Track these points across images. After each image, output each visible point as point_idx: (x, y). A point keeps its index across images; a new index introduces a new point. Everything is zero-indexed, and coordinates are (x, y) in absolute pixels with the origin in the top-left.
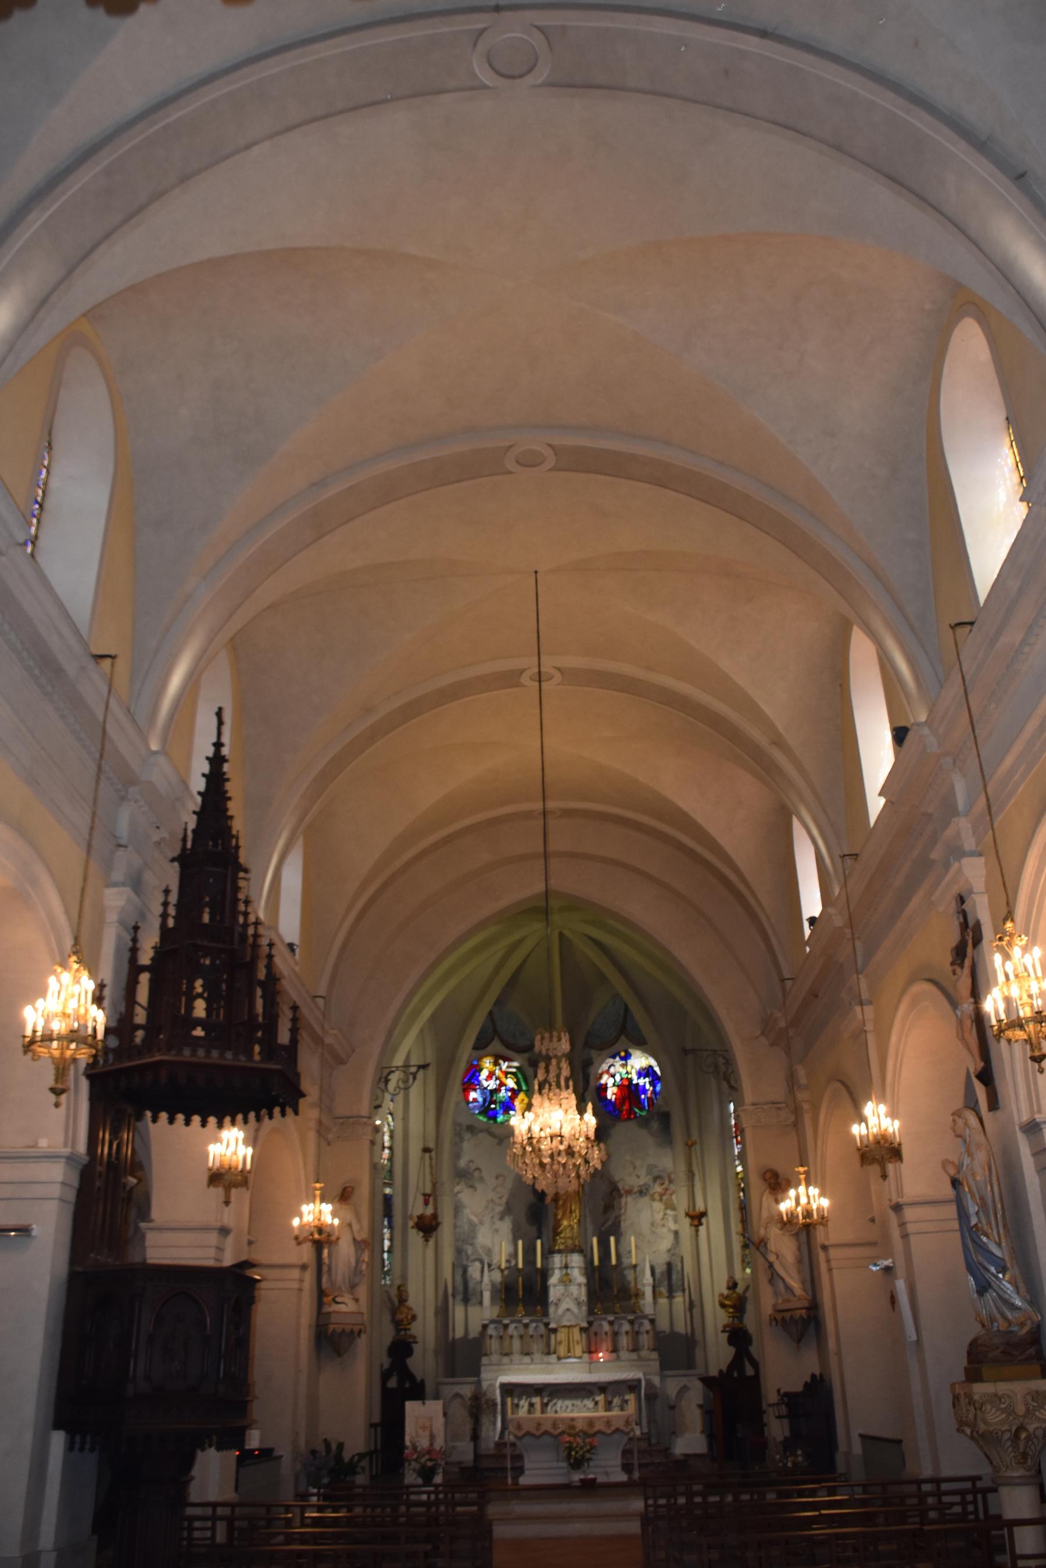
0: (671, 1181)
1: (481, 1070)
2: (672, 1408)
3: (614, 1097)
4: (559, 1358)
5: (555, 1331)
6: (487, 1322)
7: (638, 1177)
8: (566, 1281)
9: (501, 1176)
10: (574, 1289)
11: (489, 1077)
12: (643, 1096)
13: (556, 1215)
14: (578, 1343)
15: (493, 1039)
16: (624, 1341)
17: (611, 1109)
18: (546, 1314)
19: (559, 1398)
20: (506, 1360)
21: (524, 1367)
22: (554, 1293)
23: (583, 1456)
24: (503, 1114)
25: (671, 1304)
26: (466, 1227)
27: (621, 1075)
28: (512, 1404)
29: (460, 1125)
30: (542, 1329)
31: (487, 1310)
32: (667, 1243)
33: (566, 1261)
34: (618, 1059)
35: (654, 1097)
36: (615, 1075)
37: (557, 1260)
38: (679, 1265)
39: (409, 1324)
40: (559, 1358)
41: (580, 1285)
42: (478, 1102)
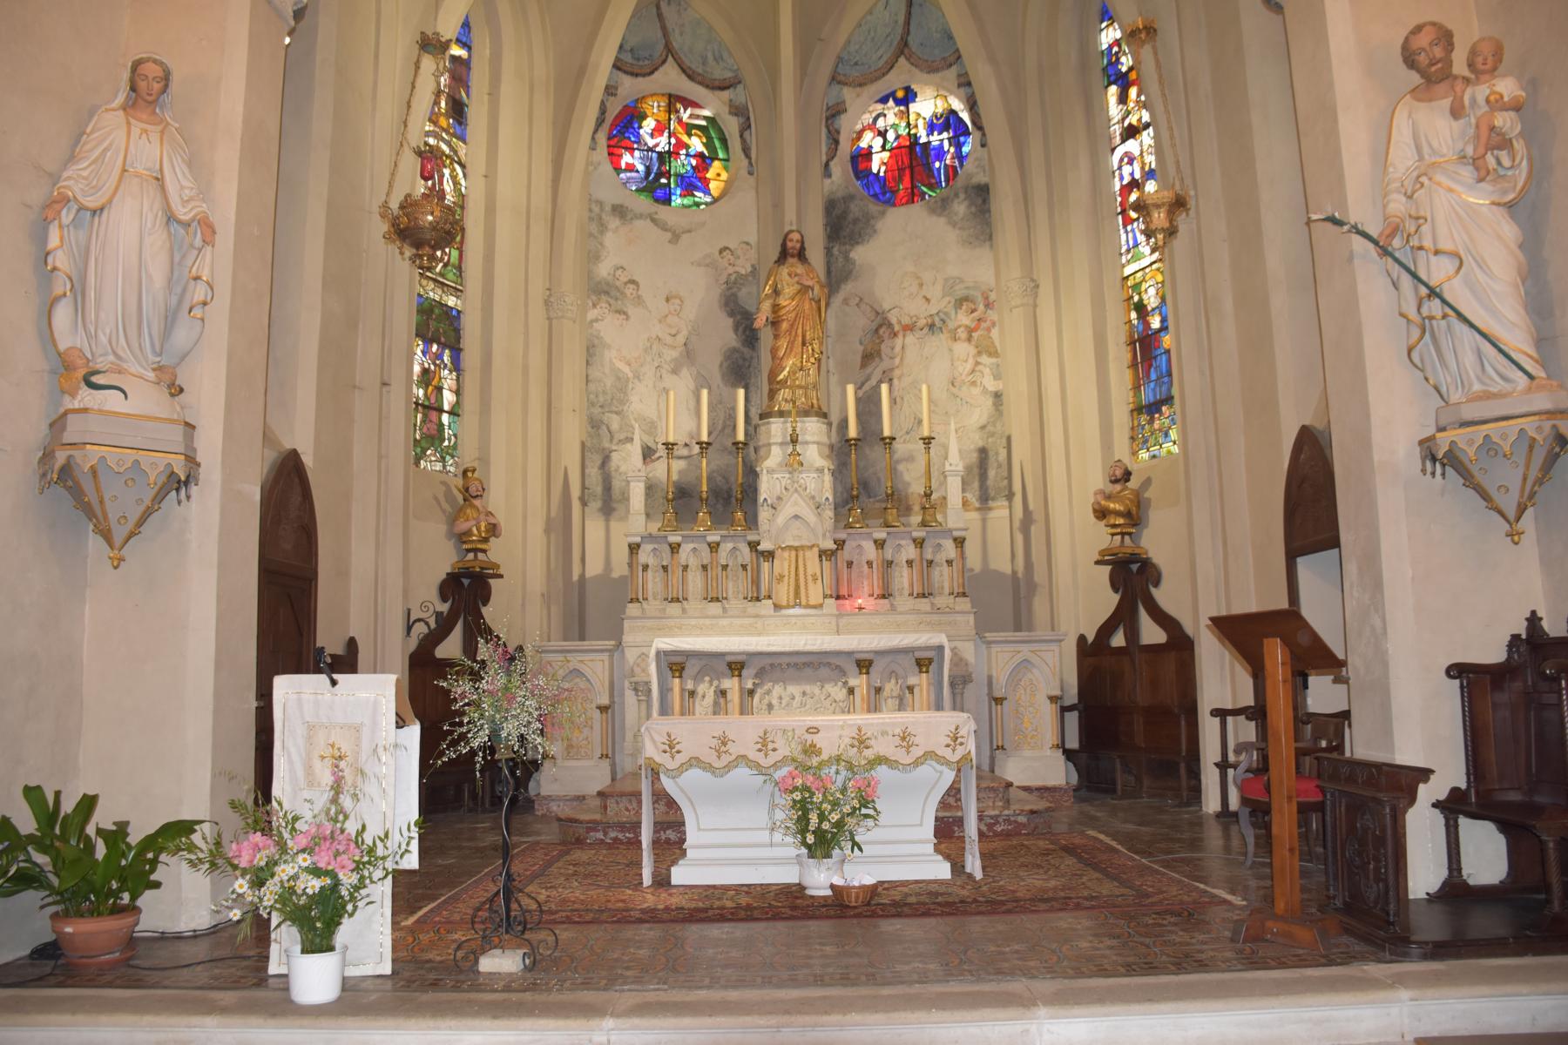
0: (988, 306)
1: (645, 117)
2: (999, 701)
3: (883, 169)
4: (777, 607)
5: (770, 555)
6: (638, 539)
7: (928, 300)
8: (794, 463)
9: (675, 297)
10: (809, 480)
11: (658, 131)
12: (937, 164)
13: (774, 351)
14: (815, 580)
15: (664, 62)
16: (903, 579)
17: (877, 190)
18: (752, 522)
19: (776, 682)
20: (674, 609)
21: (708, 622)
22: (768, 487)
23: (839, 824)
24: (681, 195)
25: (984, 520)
26: (609, 382)
27: (896, 131)
28: (682, 690)
29: (600, 203)
30: (745, 554)
31: (636, 520)
32: (980, 412)
33: (794, 430)
34: (891, 103)
35: (957, 164)
36: (886, 131)
37: (776, 429)
38: (1003, 453)
39: (486, 540)
40: (777, 607)
41: (820, 470)
42: (637, 171)
